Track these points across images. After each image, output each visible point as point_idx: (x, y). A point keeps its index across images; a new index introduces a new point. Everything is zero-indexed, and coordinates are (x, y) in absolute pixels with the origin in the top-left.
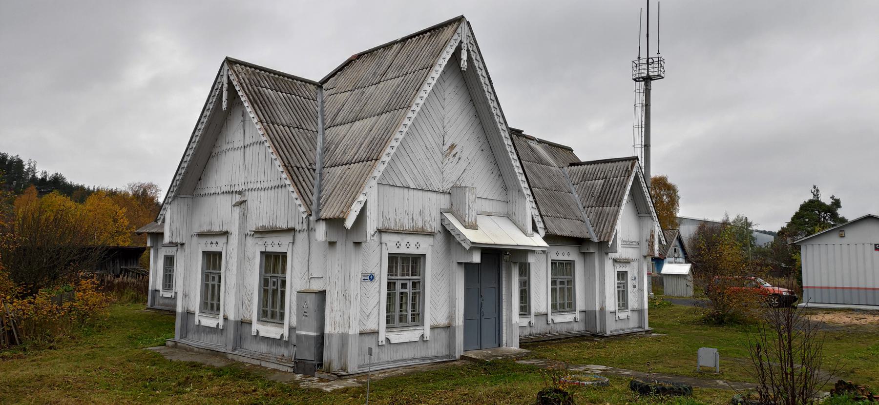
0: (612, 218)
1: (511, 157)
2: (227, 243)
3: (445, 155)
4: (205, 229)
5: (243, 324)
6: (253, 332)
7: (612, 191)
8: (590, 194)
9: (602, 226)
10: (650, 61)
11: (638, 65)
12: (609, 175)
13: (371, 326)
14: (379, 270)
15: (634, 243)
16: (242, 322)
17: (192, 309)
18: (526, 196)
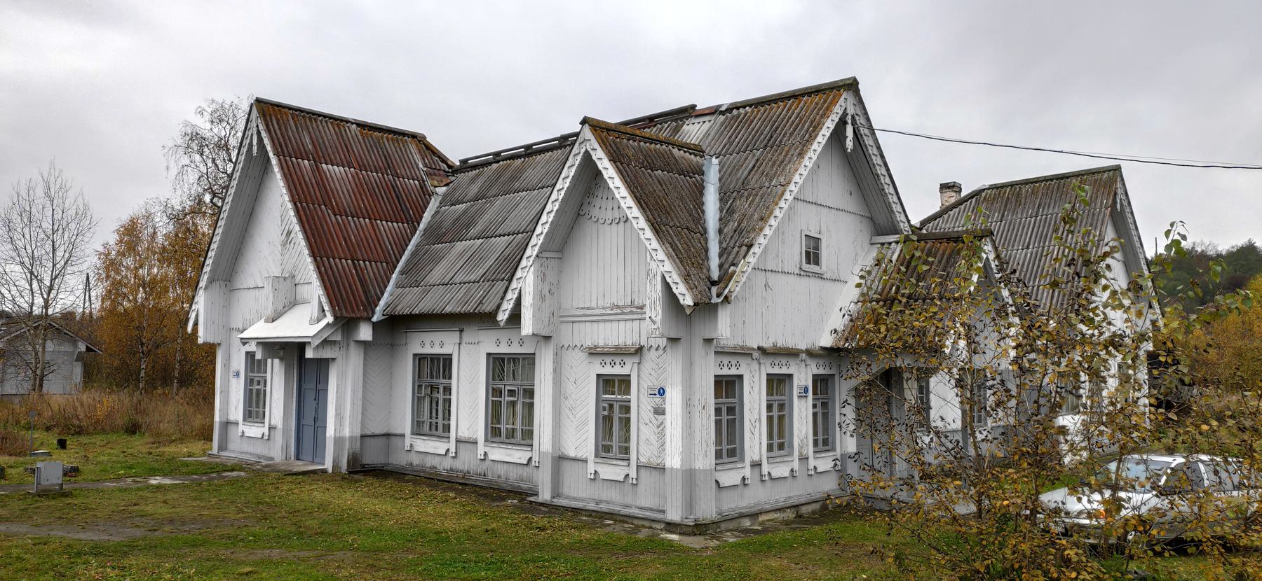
6: (479, 455)
16: (227, 423)
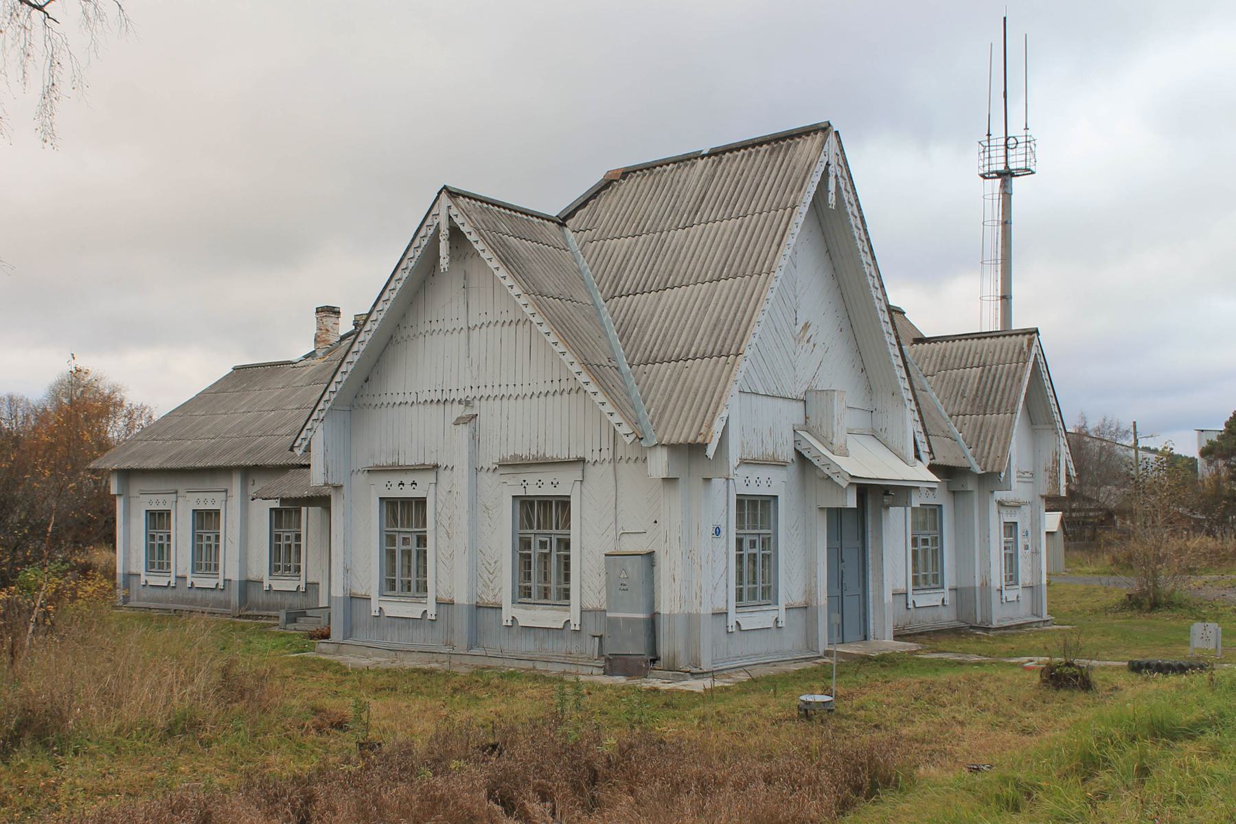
0: (1004, 433)
1: (888, 340)
2: (436, 484)
3: (798, 340)
4: (384, 460)
5: (481, 609)
7: (998, 386)
8: (958, 392)
9: (987, 447)
10: (1011, 141)
11: (987, 148)
12: (989, 359)
13: (721, 606)
14: (725, 521)
15: (1026, 475)
16: (478, 607)
17: (360, 591)
18: (907, 402)
